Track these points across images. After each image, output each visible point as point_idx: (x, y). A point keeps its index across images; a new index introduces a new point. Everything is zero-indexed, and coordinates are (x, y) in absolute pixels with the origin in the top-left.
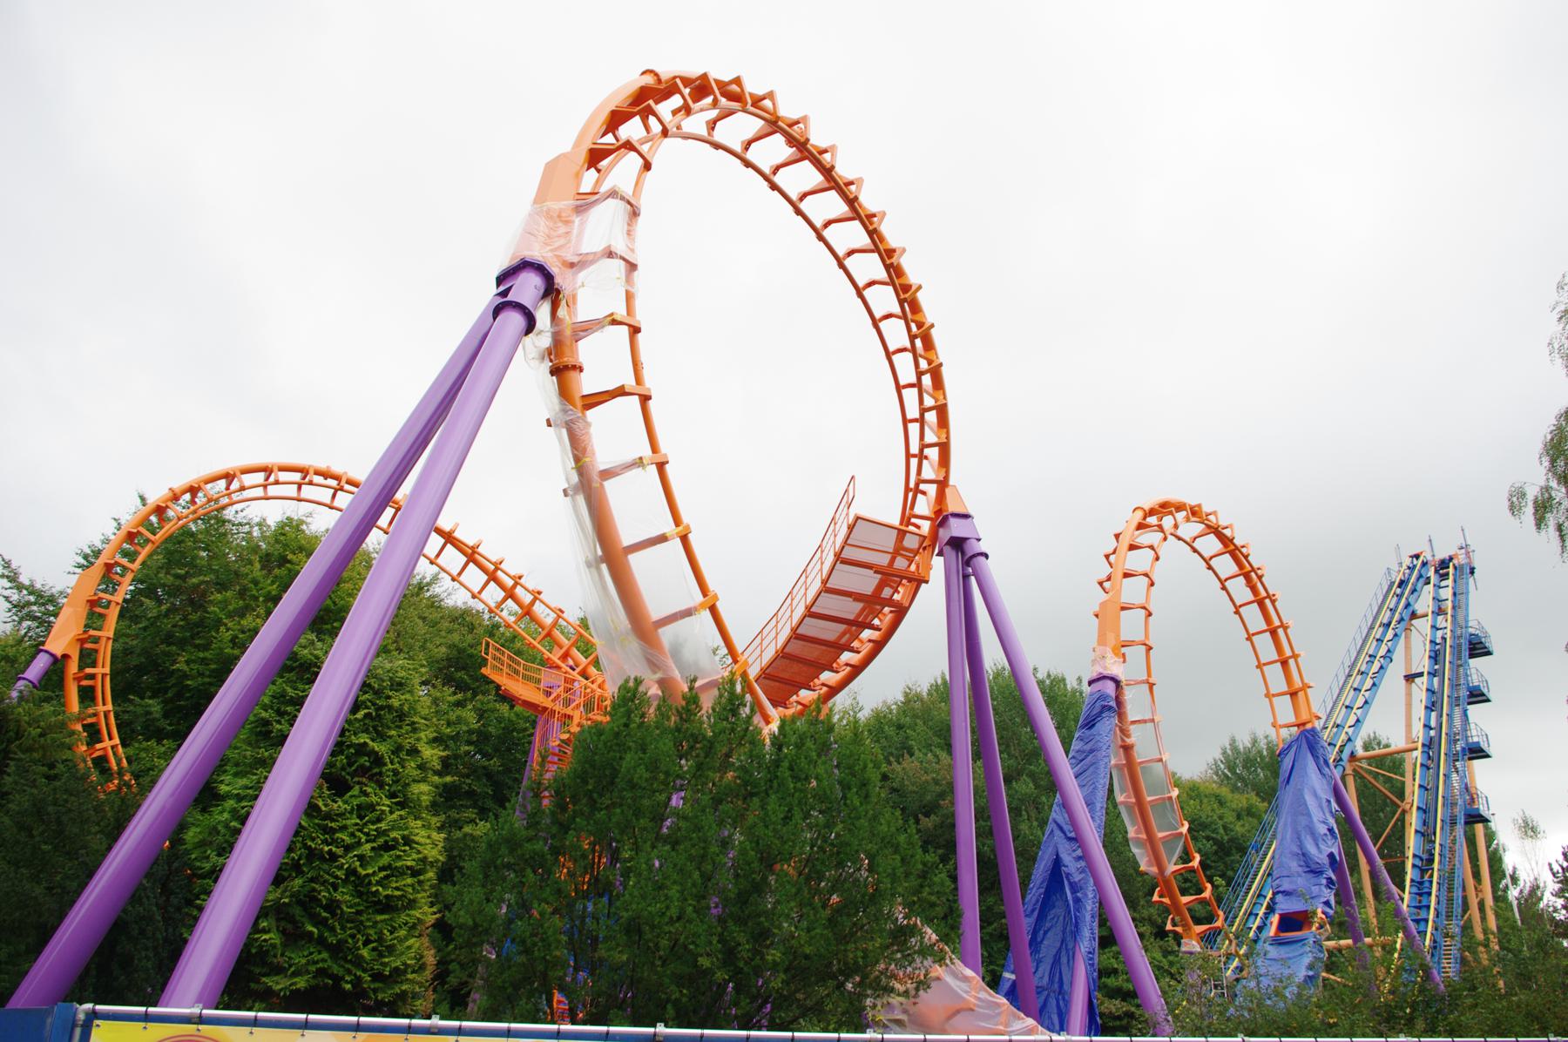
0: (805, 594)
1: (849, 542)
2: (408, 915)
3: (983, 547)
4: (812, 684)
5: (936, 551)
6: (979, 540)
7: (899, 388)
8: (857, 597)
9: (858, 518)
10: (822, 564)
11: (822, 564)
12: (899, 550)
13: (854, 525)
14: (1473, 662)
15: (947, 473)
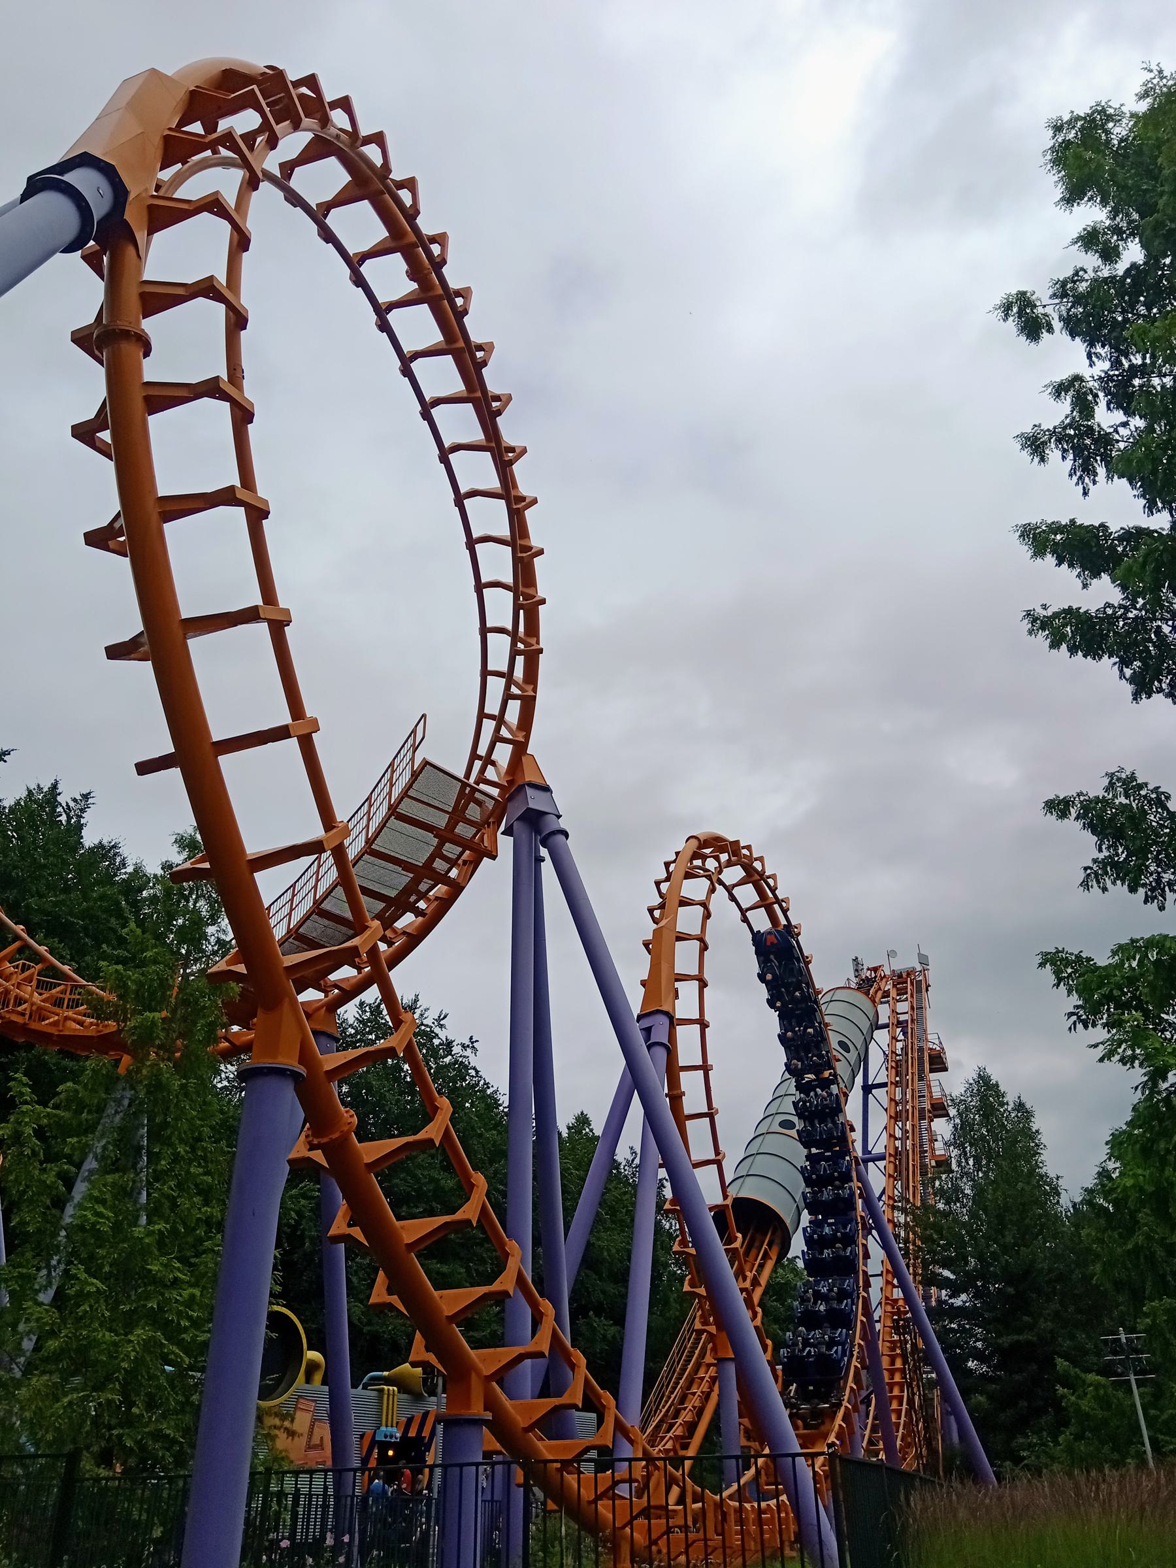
0: (290, 914)
1: (411, 793)
2: (880, 1198)
3: (563, 824)
4: (322, 982)
5: (502, 828)
6: (559, 817)
7: (484, 631)
8: (407, 866)
9: (426, 763)
10: (369, 820)
11: (369, 820)
12: (457, 815)
13: (421, 772)
14: (933, 1076)
15: (527, 737)
